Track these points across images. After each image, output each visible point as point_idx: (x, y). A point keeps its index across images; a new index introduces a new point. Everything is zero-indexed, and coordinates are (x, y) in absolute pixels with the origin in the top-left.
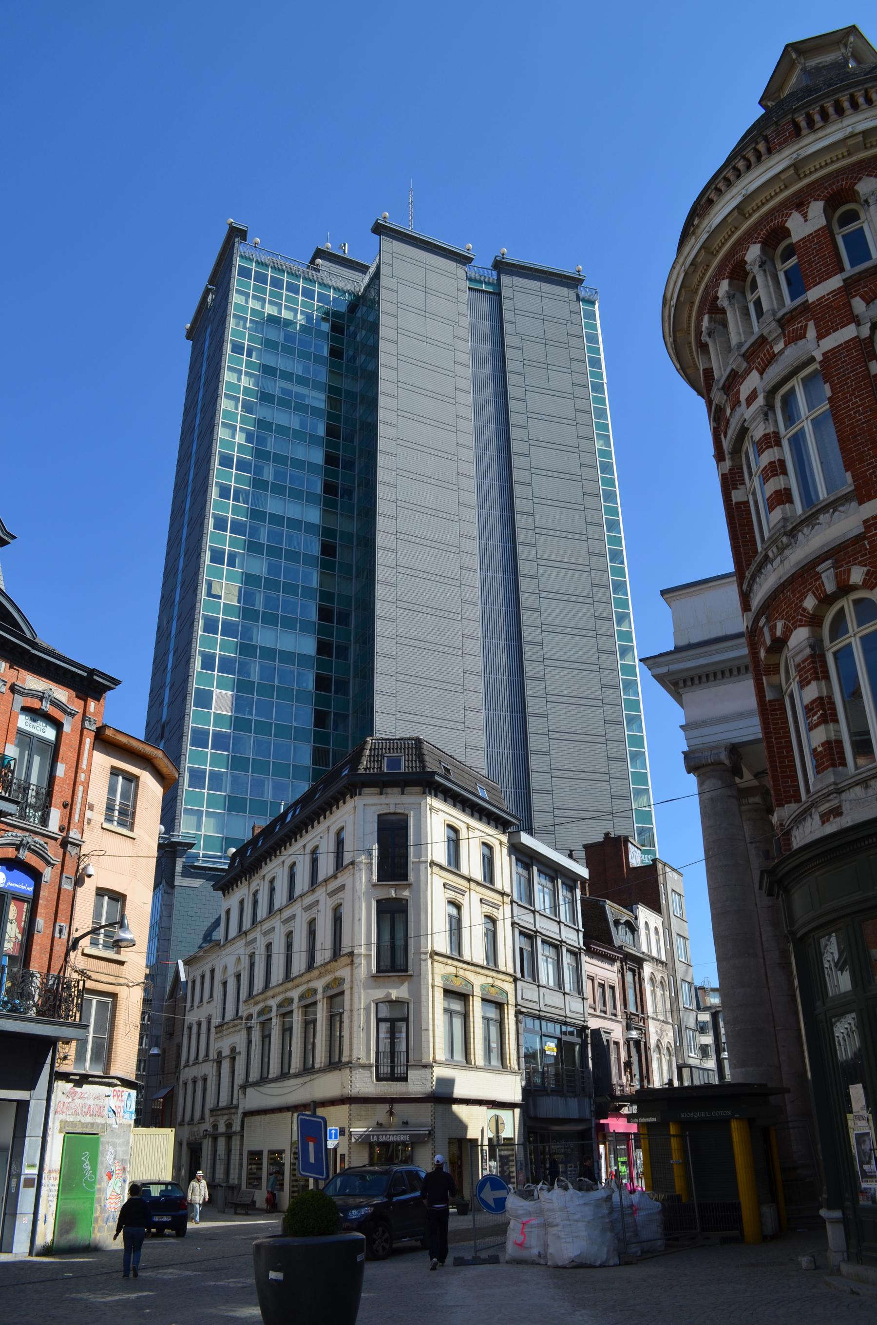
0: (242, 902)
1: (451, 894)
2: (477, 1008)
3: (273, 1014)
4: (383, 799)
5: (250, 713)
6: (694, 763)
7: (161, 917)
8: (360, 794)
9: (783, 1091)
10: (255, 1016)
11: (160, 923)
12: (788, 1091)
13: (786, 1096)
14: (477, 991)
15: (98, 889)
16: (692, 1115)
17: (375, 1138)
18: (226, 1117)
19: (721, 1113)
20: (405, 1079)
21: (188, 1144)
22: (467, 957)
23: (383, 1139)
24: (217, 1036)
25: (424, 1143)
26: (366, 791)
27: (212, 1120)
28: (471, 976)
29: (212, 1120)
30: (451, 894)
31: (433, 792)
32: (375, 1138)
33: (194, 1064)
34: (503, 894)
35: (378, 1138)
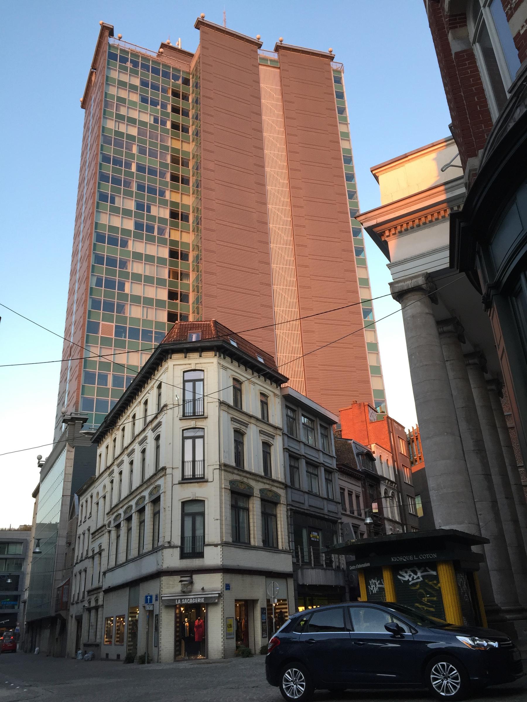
0: (107, 447)
1: (237, 426)
2: (255, 506)
3: (122, 519)
4: (186, 361)
5: (125, 337)
6: (399, 295)
7: (66, 467)
8: (171, 358)
9: (480, 541)
10: (112, 522)
11: (65, 470)
12: (487, 541)
13: (486, 545)
14: (257, 493)
15: (226, 589)
16: (401, 559)
17: (179, 602)
18: (95, 596)
19: (428, 556)
20: (201, 555)
21: (75, 617)
22: (246, 468)
23: (185, 602)
24: (93, 540)
25: (216, 604)
26: (175, 356)
27: (88, 598)
28: (252, 483)
29: (88, 598)
30: (237, 426)
31: (222, 356)
32: (179, 602)
33: (81, 561)
34: (276, 428)
35: (181, 601)
